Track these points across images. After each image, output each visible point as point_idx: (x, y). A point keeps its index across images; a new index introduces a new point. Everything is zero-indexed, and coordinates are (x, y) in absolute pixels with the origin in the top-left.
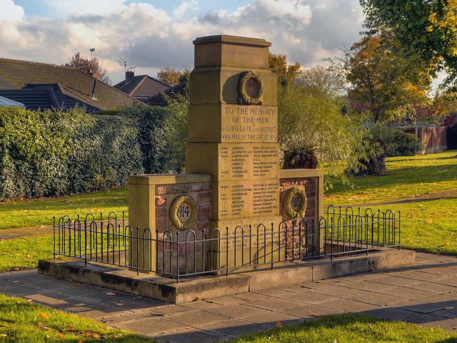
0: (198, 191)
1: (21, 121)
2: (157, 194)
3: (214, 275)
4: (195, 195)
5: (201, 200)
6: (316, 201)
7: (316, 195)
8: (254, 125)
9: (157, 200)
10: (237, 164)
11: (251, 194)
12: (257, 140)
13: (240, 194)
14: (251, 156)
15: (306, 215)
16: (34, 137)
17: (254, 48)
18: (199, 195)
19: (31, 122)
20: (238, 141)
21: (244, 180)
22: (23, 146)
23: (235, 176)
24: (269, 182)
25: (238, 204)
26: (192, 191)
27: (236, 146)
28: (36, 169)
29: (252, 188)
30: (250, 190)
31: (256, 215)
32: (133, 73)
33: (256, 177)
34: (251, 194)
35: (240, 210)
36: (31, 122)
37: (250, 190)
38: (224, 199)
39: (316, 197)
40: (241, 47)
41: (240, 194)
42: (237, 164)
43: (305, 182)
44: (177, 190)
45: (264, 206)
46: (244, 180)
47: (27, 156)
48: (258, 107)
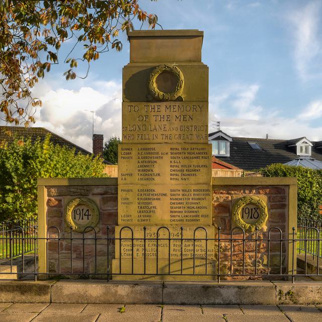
0: (101, 194)
1: (302, 175)
2: (49, 195)
3: (106, 277)
4: (97, 199)
5: (104, 204)
6: (286, 214)
7: (287, 206)
8: (170, 124)
9: (49, 201)
10: (145, 166)
11: (167, 201)
12: (174, 141)
13: (149, 199)
14: (167, 159)
15: (270, 229)
16: (311, 186)
17: (178, 40)
18: (103, 199)
19: (309, 176)
20: (147, 141)
21: (155, 184)
22: (302, 192)
23: (141, 179)
24: (193, 187)
25: (146, 209)
26: (93, 195)
27: (144, 146)
28: (313, 207)
29: (168, 193)
30: (165, 195)
31: (173, 223)
32: (74, 92)
33: (173, 182)
34: (167, 201)
35: (150, 216)
36: (309, 176)
37: (165, 195)
38: (128, 204)
39: (286, 210)
40: (159, 41)
41: (149, 199)
42: (145, 166)
43: (268, 191)
44: (74, 193)
45: (187, 214)
46: (155, 184)
47: (306, 199)
48: (177, 104)
